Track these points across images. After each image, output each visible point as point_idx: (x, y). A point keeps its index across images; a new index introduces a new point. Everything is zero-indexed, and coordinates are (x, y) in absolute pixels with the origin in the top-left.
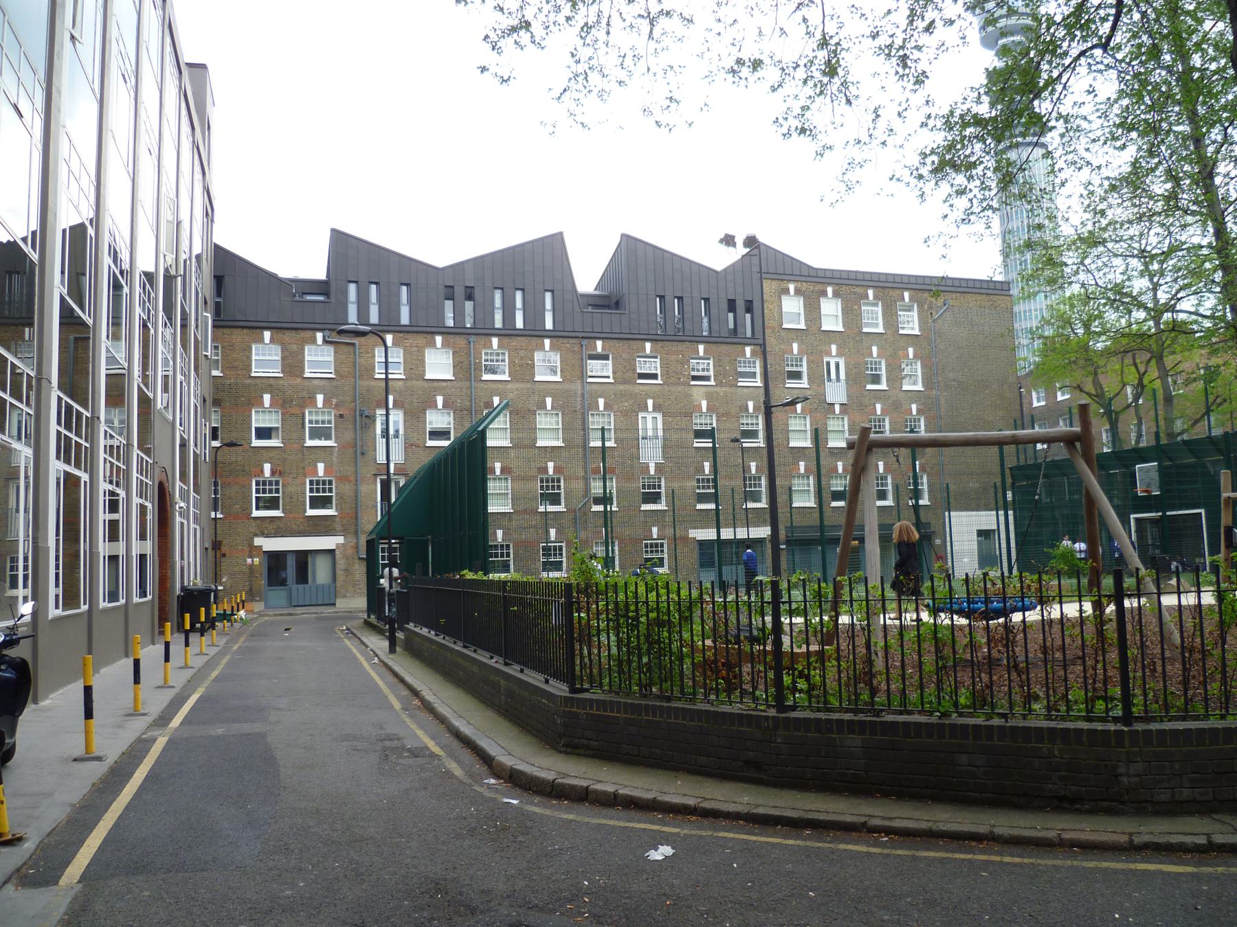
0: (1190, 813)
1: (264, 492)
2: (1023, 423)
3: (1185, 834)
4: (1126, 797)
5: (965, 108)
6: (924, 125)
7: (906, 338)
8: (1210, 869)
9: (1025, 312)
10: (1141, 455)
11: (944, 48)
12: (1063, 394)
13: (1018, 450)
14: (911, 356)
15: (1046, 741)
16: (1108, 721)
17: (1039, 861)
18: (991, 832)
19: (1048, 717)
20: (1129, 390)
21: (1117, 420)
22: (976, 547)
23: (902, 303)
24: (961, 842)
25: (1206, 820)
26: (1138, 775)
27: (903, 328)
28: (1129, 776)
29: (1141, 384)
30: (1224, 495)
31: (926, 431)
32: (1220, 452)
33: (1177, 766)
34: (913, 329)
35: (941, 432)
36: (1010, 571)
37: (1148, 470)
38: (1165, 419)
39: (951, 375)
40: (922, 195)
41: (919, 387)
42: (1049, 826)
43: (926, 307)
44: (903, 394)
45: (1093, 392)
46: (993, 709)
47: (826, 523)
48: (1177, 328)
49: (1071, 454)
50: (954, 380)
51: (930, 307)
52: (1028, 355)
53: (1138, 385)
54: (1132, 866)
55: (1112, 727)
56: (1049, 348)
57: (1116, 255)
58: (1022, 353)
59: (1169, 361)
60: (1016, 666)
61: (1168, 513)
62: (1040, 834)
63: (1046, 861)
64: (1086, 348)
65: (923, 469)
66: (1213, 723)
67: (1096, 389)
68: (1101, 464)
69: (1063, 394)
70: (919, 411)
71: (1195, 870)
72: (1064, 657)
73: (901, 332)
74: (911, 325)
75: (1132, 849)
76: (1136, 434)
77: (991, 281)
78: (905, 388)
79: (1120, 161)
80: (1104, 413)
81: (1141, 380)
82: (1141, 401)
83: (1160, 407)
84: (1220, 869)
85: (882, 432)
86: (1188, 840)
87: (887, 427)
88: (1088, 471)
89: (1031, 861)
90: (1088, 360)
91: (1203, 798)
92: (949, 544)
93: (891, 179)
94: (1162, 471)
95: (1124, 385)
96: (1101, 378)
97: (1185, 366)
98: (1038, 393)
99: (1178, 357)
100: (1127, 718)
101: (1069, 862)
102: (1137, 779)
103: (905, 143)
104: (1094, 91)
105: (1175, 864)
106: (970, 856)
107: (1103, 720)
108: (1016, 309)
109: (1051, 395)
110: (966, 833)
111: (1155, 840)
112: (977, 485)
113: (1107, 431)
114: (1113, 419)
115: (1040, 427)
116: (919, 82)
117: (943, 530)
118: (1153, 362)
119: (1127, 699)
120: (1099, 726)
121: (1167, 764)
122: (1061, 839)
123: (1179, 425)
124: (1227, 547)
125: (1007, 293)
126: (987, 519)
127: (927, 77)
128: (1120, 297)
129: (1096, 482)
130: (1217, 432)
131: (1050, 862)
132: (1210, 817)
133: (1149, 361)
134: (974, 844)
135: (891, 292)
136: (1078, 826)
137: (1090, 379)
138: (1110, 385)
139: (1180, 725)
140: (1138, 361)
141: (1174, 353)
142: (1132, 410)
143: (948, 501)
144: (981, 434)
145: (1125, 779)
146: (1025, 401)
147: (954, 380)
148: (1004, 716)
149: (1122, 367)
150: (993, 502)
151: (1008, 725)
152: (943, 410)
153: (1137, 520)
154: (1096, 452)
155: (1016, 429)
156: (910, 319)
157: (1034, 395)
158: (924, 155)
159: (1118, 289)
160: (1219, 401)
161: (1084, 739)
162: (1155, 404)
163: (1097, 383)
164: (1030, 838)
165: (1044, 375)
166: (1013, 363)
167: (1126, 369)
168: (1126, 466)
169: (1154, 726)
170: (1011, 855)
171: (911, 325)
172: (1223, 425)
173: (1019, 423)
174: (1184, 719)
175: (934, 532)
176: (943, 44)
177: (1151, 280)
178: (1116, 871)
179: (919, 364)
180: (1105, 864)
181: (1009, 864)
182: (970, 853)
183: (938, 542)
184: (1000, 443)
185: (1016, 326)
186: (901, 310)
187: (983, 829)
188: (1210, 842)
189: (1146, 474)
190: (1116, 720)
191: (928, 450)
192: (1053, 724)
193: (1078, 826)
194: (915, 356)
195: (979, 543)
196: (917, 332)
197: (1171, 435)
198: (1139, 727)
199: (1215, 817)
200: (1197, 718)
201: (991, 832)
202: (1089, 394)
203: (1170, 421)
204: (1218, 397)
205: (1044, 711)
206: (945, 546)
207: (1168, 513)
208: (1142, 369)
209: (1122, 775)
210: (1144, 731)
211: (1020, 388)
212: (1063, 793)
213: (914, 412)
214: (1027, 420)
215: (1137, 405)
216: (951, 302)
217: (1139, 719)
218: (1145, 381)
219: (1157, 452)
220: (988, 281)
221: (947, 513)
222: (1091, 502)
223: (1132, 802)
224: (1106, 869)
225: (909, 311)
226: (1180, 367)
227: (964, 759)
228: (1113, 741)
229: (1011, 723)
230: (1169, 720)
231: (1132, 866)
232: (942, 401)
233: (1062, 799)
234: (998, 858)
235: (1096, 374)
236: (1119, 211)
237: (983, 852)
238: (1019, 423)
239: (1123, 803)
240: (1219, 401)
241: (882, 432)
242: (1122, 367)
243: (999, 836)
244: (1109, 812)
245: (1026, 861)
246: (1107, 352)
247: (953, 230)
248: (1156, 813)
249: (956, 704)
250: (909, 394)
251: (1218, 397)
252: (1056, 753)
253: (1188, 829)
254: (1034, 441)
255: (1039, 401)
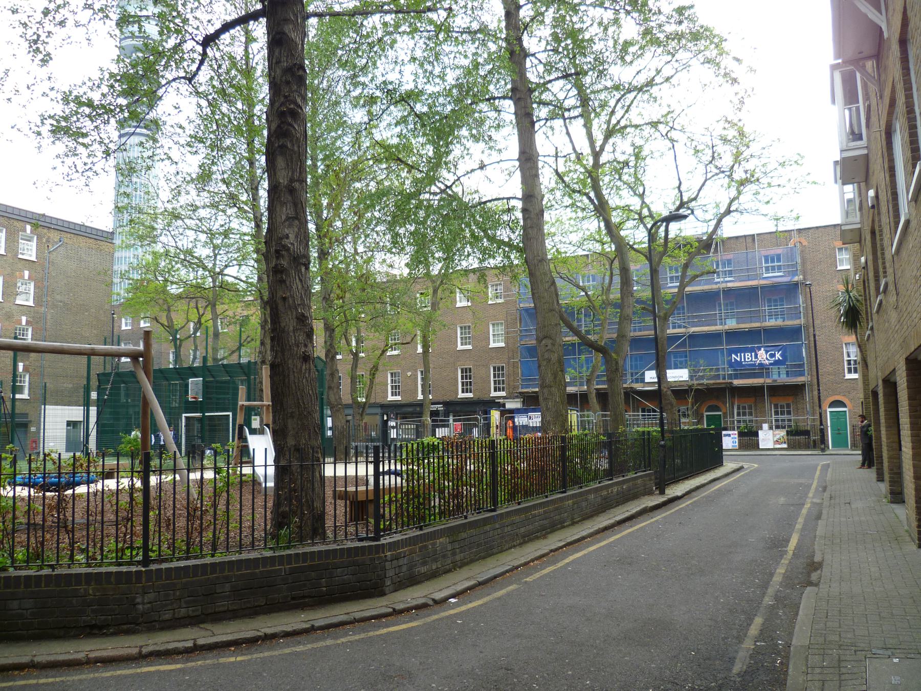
0: (185, 626)
1: (744, 414)
2: (113, 341)
3: (179, 641)
4: (141, 620)
5: (81, 91)
6: (44, 94)
7: (23, 262)
8: (193, 664)
9: (125, 258)
10: (192, 372)
11: (69, 41)
12: (145, 322)
13: (105, 361)
14: (26, 277)
15: (83, 584)
16: (133, 565)
17: (68, 678)
18: (32, 661)
19: (89, 565)
20: (192, 325)
21: (180, 345)
22: (65, 434)
23: (23, 234)
24: (5, 673)
25: (195, 629)
26: (150, 603)
27: (23, 254)
28: (143, 604)
29: (199, 322)
30: (240, 403)
31: (32, 339)
32: (246, 375)
33: (178, 593)
34: (31, 256)
35: (45, 341)
36: (486, 461)
37: (197, 384)
38: (213, 349)
39: (58, 297)
40: (39, 148)
41: (31, 303)
42: (80, 650)
43: (44, 240)
44: (14, 307)
45: (166, 323)
46: (43, 562)
47: (17, 411)
48: (224, 286)
49: (135, 366)
50: (61, 302)
51: (48, 241)
52: (121, 290)
53: (198, 322)
54: (139, 671)
55: (134, 569)
56: (137, 287)
57: (188, 228)
58: (116, 289)
59: (220, 308)
60: (66, 527)
61: (206, 414)
62: (71, 657)
63: (74, 678)
64: (165, 291)
65: (26, 369)
66: (208, 560)
67: (168, 322)
68: (161, 377)
69: (145, 322)
70: (28, 323)
71: (183, 666)
72: (117, 519)
73: (20, 256)
74: (29, 253)
75: (142, 657)
76: (192, 357)
77: (83, 225)
78: (18, 302)
79: (192, 164)
80: (172, 340)
81: (200, 319)
82: (198, 334)
83: (210, 340)
84: (199, 663)
85: (24, 339)
86: (180, 645)
87: (30, 336)
88: (146, 380)
89: (61, 679)
90: (165, 300)
91: (195, 614)
92: (42, 431)
93: (12, 127)
94: (205, 384)
95: (188, 321)
96: (173, 315)
97: (230, 313)
98: (126, 319)
99: (226, 307)
100: (146, 561)
101: (92, 676)
102: (149, 605)
103: (27, 104)
104: (179, 107)
105: (169, 664)
106: (10, 684)
107: (130, 563)
108: (117, 255)
109: (136, 322)
110: (10, 665)
111: (157, 649)
112: (71, 386)
113: (173, 352)
114: (177, 345)
115: (125, 344)
116: (44, 62)
117: (39, 421)
118: (209, 308)
119: (146, 548)
120: (124, 569)
121: (171, 592)
122: (88, 659)
123: (221, 354)
124: (239, 438)
125: (110, 241)
126: (76, 413)
127: (51, 59)
128: (188, 258)
129: (151, 389)
130: (244, 360)
131: (76, 678)
132: (199, 627)
133: (207, 306)
134: (16, 672)
135: (16, 223)
136: (104, 646)
137: (165, 314)
138: (178, 321)
139: (182, 564)
140: (199, 306)
141: (223, 304)
142: (192, 339)
143: (44, 397)
144: (66, 345)
145: (140, 607)
146: (116, 325)
147: (61, 302)
148: (52, 567)
149: (189, 308)
150: (82, 400)
151: (54, 573)
152: (48, 324)
153: (186, 417)
154: (156, 367)
155: (113, 345)
156: (29, 248)
157: (123, 320)
158: (43, 119)
159: (189, 252)
160: (249, 339)
161: (113, 579)
162: (207, 336)
163: (169, 319)
164: (63, 661)
165: (131, 307)
166: (110, 295)
167: (191, 310)
168: (182, 379)
169: (164, 566)
170: (47, 677)
171: (29, 253)
172: (249, 356)
173: (109, 340)
174: (187, 558)
175: (31, 421)
176: (69, 37)
177: (214, 251)
178: (126, 676)
179: (32, 284)
180: (119, 672)
181: (43, 684)
182: (11, 681)
183: (33, 429)
184: (91, 353)
185: (115, 268)
186: (22, 239)
187: (25, 659)
188: (195, 645)
189: (195, 384)
190: (139, 562)
191: (33, 355)
192: (90, 570)
193: (104, 646)
194: (30, 278)
195: (68, 431)
196: (34, 258)
197: (215, 359)
198: (153, 567)
199: (202, 626)
200: (196, 557)
201: (32, 661)
202: (162, 325)
203: (215, 350)
204: (248, 337)
205: (84, 561)
206: (39, 433)
207: (206, 414)
208: (201, 312)
209: (138, 604)
210: (157, 570)
211: (113, 314)
212: (94, 622)
213: (24, 323)
214: (115, 339)
215: (195, 337)
216: (65, 240)
217: (154, 561)
218: (203, 321)
219: (204, 371)
220: (81, 225)
221: (43, 406)
222: (146, 403)
223: (146, 623)
224: (119, 676)
225: (29, 241)
226: (227, 313)
227: (15, 604)
228: (134, 579)
229: (58, 571)
230: (177, 560)
231: (139, 671)
232: (49, 317)
233: (93, 627)
234: (34, 682)
235: (169, 310)
236: (191, 195)
237: (24, 678)
238: (109, 340)
239: (137, 624)
240: (249, 339)
241: (24, 339)
242: (189, 308)
243: (38, 663)
244: (128, 632)
245: (58, 679)
246: (179, 297)
247: (59, 180)
248: (162, 629)
249: (14, 560)
250: (21, 308)
251: (248, 337)
252: (91, 592)
253: (177, 637)
254: (120, 355)
255: (126, 326)
